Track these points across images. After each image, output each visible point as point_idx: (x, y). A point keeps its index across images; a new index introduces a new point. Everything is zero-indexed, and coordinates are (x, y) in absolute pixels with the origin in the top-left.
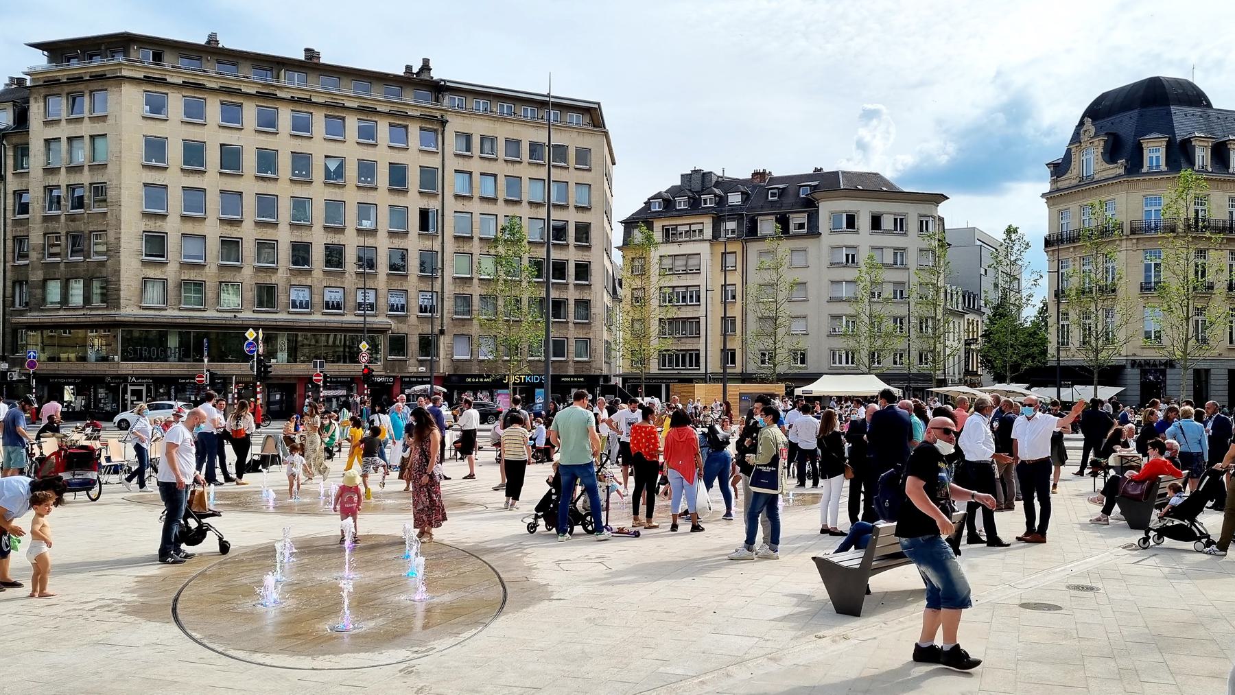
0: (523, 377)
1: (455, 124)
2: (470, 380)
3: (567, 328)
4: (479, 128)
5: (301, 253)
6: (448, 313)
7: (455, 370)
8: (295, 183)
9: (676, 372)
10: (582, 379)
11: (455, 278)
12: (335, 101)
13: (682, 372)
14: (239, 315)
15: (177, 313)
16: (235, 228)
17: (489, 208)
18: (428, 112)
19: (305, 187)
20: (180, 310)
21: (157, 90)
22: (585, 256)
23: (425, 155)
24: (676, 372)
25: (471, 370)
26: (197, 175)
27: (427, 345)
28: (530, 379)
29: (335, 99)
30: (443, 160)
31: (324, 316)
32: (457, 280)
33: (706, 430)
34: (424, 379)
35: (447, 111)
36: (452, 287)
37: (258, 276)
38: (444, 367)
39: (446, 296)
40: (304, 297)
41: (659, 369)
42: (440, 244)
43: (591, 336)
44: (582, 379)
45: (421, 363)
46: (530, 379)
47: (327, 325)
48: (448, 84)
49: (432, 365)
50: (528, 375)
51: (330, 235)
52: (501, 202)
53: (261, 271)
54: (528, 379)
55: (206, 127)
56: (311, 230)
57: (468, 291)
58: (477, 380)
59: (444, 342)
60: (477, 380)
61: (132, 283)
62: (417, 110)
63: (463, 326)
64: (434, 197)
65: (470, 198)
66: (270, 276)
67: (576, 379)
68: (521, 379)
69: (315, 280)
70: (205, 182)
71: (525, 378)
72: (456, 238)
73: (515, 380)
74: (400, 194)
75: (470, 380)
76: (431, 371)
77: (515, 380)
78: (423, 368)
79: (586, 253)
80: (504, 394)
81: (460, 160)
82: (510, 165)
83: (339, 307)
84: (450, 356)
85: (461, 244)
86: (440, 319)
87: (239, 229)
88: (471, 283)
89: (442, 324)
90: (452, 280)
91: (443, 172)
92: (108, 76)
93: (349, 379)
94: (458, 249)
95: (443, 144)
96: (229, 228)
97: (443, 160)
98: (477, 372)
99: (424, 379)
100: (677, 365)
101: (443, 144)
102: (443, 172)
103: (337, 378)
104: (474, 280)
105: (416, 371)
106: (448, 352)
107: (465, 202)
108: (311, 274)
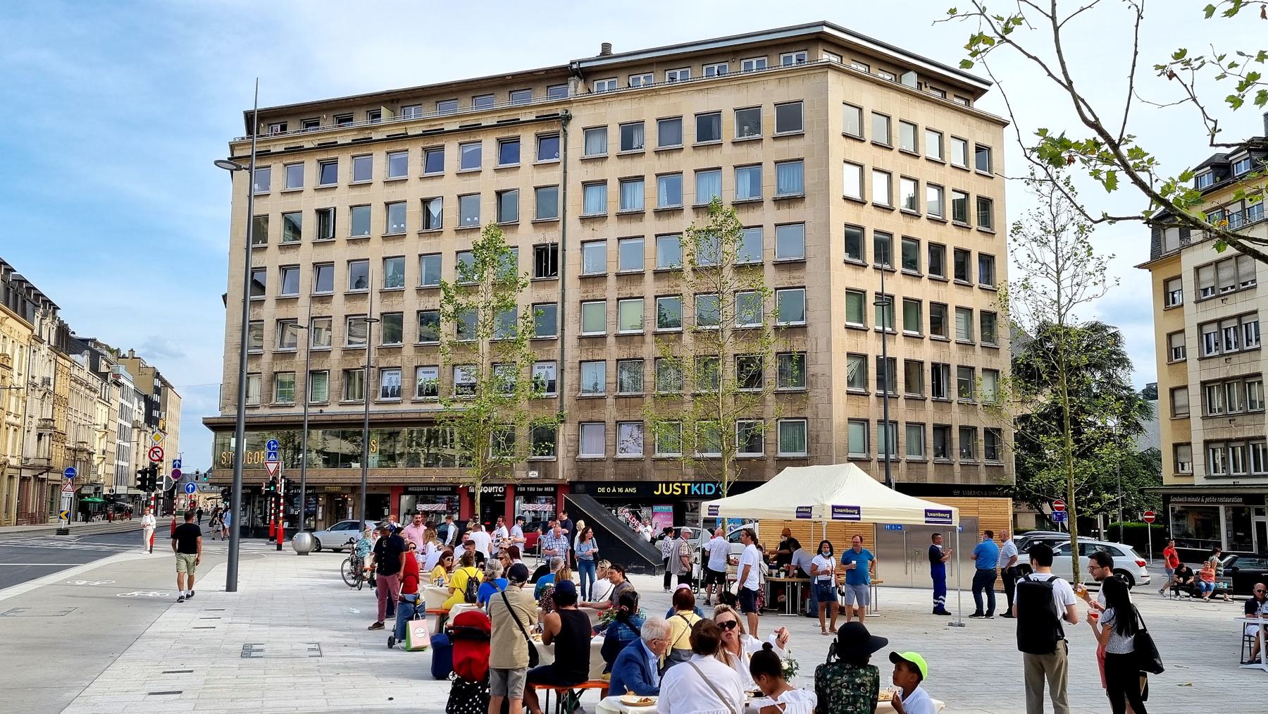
0: (686, 485)
1: (583, 117)
2: (603, 490)
3: (763, 402)
4: (615, 114)
5: (393, 323)
6: (571, 390)
7: (580, 475)
8: (546, 227)
9: (1230, 482)
10: (633, 490)
11: (581, 338)
12: (437, 128)
13: (1242, 482)
14: (325, 410)
15: (267, 411)
16: (326, 305)
17: (545, 239)
18: (546, 111)
19: (398, 243)
20: (414, 402)
21: (295, 161)
22: (794, 278)
23: (541, 170)
24: (1230, 482)
25: (603, 475)
26: (292, 250)
27: (544, 438)
28: (699, 488)
29: (433, 126)
30: (565, 172)
31: (341, 407)
32: (584, 341)
33: (480, 576)
34: (546, 489)
35: (570, 102)
36: (576, 352)
37: (346, 360)
38: (564, 470)
39: (567, 365)
40: (397, 381)
41: (1207, 478)
42: (560, 291)
43: (808, 413)
44: (633, 490)
45: (533, 465)
46: (699, 488)
47: (403, 416)
48: (582, 65)
49: (547, 468)
50: (695, 483)
51: (424, 299)
52: (612, 219)
53: (349, 354)
54: (694, 489)
55: (481, 174)
56: (402, 296)
57: (756, 349)
58: (614, 490)
59: (565, 434)
60: (614, 490)
61: (232, 381)
62: (531, 113)
63: (592, 408)
64: (552, 226)
65: (759, 203)
66: (358, 360)
67: (621, 490)
68: (683, 488)
69: (405, 359)
70: (299, 257)
71: (689, 488)
72: (582, 278)
73: (673, 490)
74: (508, 231)
75: (603, 490)
76: (546, 476)
77: (673, 490)
78: (535, 472)
79: (796, 274)
80: (663, 513)
81: (590, 167)
82: (663, 157)
83: (434, 392)
84: (572, 454)
85: (590, 287)
86: (559, 400)
87: (329, 305)
88: (604, 344)
89: (562, 406)
90: (576, 342)
91: (565, 189)
92: (521, 120)
93: (552, 489)
94: (586, 295)
95: (565, 150)
96: (319, 305)
97: (565, 172)
98: (612, 478)
99: (546, 489)
100: (1257, 468)
101: (565, 150)
102: (565, 189)
103: (436, 487)
104: (608, 339)
105: (524, 476)
106: (570, 448)
107: (597, 226)
108: (400, 352)
